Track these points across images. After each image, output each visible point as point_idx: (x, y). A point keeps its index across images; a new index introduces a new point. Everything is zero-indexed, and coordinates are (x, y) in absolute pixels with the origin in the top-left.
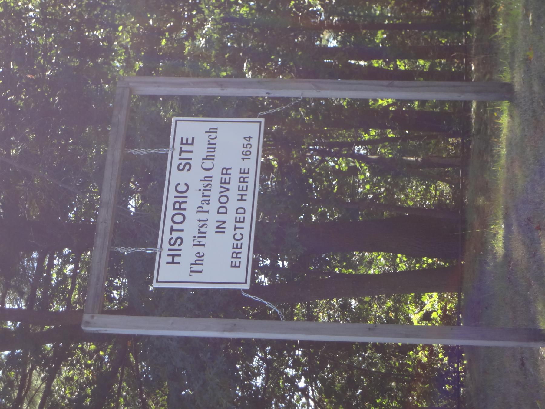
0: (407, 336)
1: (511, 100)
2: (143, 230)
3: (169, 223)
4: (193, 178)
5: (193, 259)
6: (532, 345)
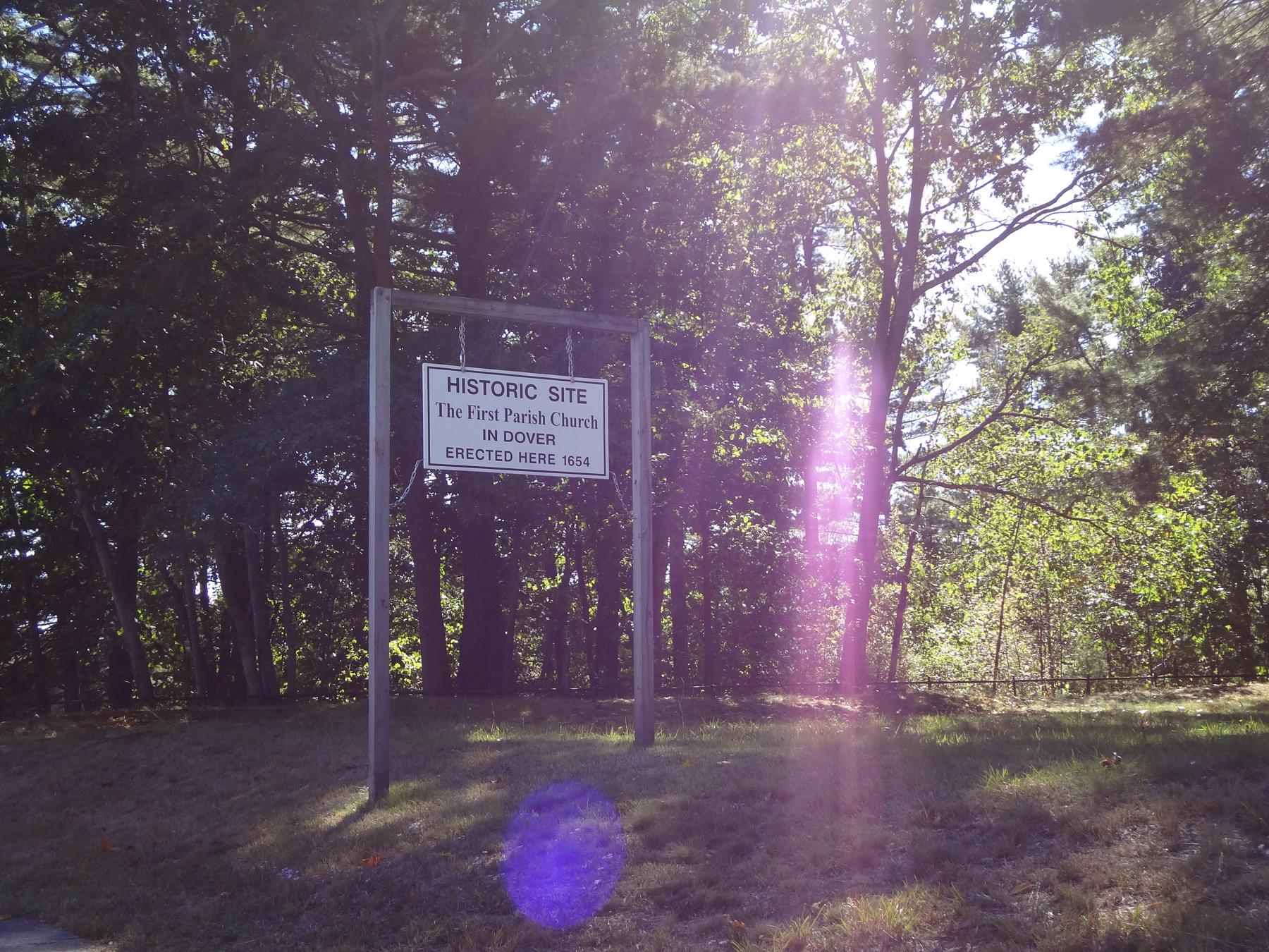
0: (377, 642)
1: (636, 743)
2: (486, 353)
3: (492, 378)
4: (543, 404)
5: (454, 406)
6: (371, 778)
